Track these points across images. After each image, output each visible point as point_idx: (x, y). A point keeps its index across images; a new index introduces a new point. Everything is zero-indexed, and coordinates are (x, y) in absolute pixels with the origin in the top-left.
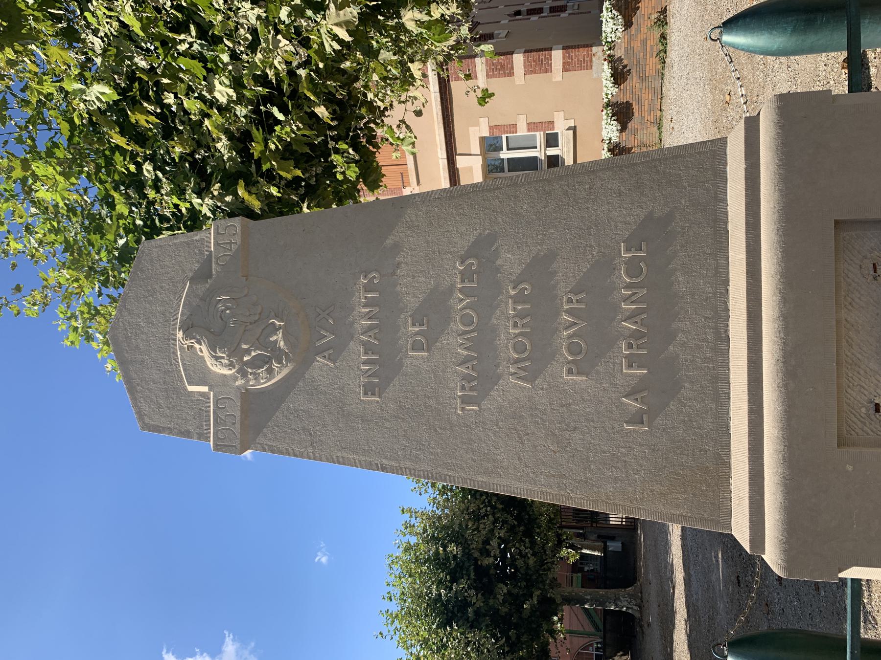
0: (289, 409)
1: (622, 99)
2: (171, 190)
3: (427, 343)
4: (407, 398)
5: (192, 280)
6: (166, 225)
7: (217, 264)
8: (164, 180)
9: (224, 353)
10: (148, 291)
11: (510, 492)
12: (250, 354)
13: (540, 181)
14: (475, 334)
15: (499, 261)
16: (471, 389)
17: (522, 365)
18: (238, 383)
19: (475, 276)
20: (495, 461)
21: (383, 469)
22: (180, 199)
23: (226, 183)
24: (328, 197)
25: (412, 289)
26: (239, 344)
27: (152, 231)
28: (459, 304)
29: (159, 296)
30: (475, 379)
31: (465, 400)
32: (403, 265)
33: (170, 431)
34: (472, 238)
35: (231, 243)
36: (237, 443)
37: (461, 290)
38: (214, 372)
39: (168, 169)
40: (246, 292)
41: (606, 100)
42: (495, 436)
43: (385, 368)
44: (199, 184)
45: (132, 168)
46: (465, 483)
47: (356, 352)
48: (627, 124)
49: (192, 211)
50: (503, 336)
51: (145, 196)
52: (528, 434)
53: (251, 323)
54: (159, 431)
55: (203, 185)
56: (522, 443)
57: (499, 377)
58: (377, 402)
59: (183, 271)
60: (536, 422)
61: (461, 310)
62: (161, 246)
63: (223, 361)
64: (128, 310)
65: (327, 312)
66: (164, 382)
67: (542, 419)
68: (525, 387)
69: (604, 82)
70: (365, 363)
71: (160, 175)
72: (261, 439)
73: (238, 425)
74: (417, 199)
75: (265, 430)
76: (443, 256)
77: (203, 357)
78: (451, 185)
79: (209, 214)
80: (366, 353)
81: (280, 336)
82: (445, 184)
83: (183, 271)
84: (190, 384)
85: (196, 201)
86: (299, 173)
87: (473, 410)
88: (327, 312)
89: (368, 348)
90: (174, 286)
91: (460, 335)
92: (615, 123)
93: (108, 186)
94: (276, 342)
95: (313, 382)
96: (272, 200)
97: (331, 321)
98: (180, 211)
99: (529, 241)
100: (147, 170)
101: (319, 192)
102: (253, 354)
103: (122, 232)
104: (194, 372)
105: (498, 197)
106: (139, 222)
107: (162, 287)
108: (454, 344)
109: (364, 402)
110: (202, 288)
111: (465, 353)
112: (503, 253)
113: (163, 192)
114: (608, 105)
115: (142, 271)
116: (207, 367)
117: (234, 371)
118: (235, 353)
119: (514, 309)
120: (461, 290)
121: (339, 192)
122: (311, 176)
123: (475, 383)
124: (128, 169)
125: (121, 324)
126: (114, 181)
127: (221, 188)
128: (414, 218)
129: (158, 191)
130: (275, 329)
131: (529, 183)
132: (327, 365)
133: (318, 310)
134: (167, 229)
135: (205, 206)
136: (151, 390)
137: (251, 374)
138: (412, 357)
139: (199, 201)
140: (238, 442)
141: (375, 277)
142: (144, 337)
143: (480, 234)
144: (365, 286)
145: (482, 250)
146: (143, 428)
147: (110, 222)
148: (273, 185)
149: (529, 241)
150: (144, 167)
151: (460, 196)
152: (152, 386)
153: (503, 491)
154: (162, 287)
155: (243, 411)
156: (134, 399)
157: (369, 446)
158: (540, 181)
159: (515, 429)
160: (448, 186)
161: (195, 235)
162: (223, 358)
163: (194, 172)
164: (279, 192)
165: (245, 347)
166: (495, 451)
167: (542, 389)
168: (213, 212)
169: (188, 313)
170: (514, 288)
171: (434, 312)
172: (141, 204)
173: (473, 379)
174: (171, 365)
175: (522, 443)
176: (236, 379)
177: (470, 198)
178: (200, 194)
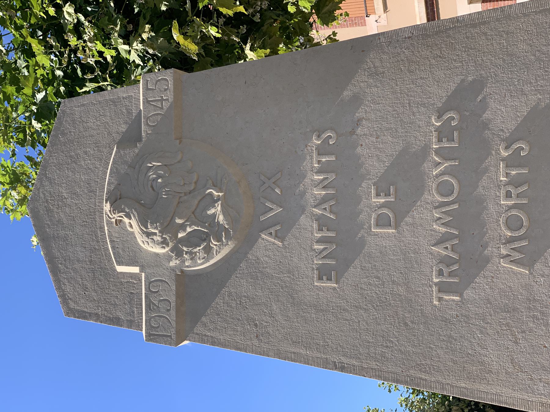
0: (230, 294)
2: (95, 35)
3: (395, 216)
4: (370, 284)
5: (121, 144)
6: (89, 76)
7: (148, 125)
8: (87, 24)
9: (156, 228)
10: (71, 157)
11: (500, 402)
12: (185, 230)
13: (540, 12)
14: (456, 206)
15: (487, 115)
16: (451, 274)
17: (516, 245)
18: (172, 264)
19: (456, 134)
20: (482, 363)
21: (342, 369)
22: (104, 45)
23: (156, 23)
24: (275, 34)
25: (375, 156)
26: (173, 219)
27: (72, 84)
28: (436, 169)
29: (82, 163)
30: (455, 262)
31: (443, 288)
32: (364, 122)
33: (97, 317)
34: (453, 87)
35: (162, 100)
36: (172, 332)
37: (438, 152)
38: (146, 251)
39: (89, 9)
40: (179, 157)
42: (481, 333)
43: (343, 249)
44: (126, 27)
45: (52, 11)
46: (443, 389)
47: (308, 228)
49: (118, 58)
50: (492, 208)
51: (65, 43)
52: (523, 332)
53: (185, 194)
54: (85, 318)
55: (130, 27)
56: (516, 343)
57: (488, 260)
58: (334, 289)
59: (109, 134)
60: (534, 317)
61: (437, 176)
62: (83, 105)
63: (155, 238)
64: (49, 179)
65: (273, 180)
66: (91, 261)
67: (542, 313)
68: (520, 273)
70: (319, 241)
71: (82, 18)
72: (199, 329)
73: (173, 312)
74: (382, 39)
75: (203, 319)
76: (415, 110)
77: (133, 233)
78: (428, 20)
79: (138, 61)
80: (320, 230)
81: (219, 208)
82: (420, 17)
83: (109, 134)
84: (119, 263)
85: (123, 48)
86: (241, 9)
87: (453, 300)
88: (273, 180)
89: (322, 223)
90: (99, 151)
91: (436, 208)
93: (24, 32)
94: (214, 215)
95: (259, 263)
96: (208, 42)
97: (278, 191)
98: (105, 59)
99: (527, 88)
100: (68, 13)
101: (264, 28)
102: (189, 230)
103: (40, 84)
104: (123, 250)
105: (485, 34)
106: (59, 73)
107: (86, 153)
108: (429, 218)
109: (319, 288)
110: (131, 153)
111: (443, 230)
112: (492, 104)
113: (86, 38)
115: (63, 134)
116: (140, 248)
117: (167, 249)
118: (169, 228)
119: (507, 175)
120: (438, 152)
121: (288, 27)
122: (256, 12)
123: (456, 267)
124: (46, 13)
125: (42, 195)
126: (31, 26)
127: (152, 30)
128: (378, 64)
129: (80, 37)
130: (213, 201)
131: (525, 15)
132: (274, 244)
133: (262, 178)
134: (91, 80)
135: (132, 53)
136: (75, 270)
137: (187, 253)
138: (376, 235)
139: (127, 47)
140: (173, 331)
141: (330, 137)
142: (67, 210)
143: (463, 81)
144: (318, 148)
145: (466, 99)
146: (67, 314)
147: (27, 74)
148: (212, 25)
149: (527, 88)
150: (65, 9)
151: (437, 33)
152: (77, 266)
153: (492, 400)
154: (86, 153)
155: (179, 296)
156: (58, 281)
157: (325, 341)
158: (540, 12)
159: (507, 325)
160: (425, 21)
161: (122, 91)
162: (155, 234)
163: (119, 12)
164: (218, 32)
165: (179, 221)
166: (482, 352)
167: (543, 276)
168: (142, 58)
169: (116, 182)
170: (507, 148)
171: (404, 180)
172: (62, 54)
173: (454, 262)
174: (98, 242)
175: (516, 343)
176: (170, 259)
177: (448, 37)
178: (127, 38)
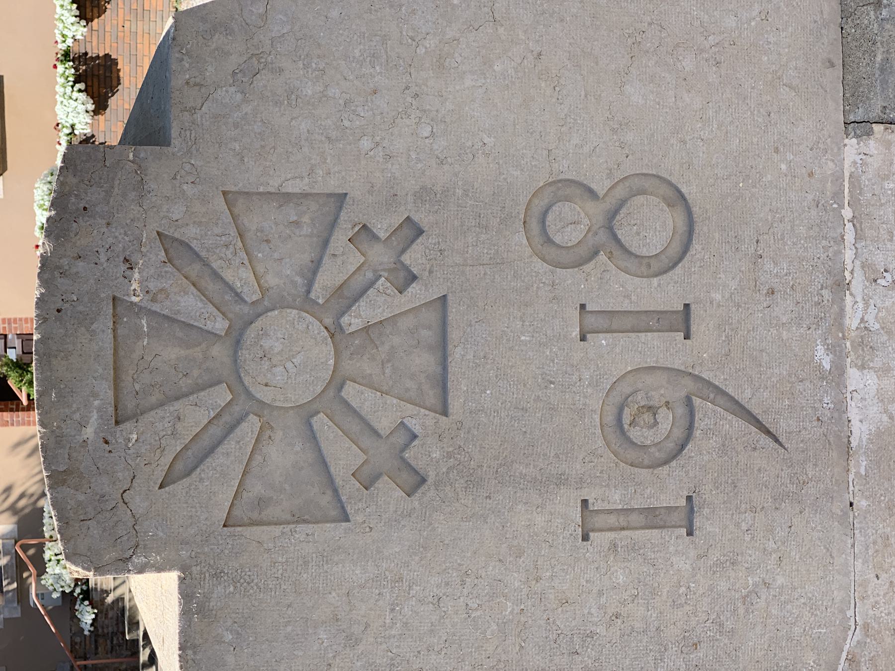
1: (96, 49)
41: (62, 46)
48: (107, 99)
69: (59, 10)
92: (82, 96)
114: (66, 55)
